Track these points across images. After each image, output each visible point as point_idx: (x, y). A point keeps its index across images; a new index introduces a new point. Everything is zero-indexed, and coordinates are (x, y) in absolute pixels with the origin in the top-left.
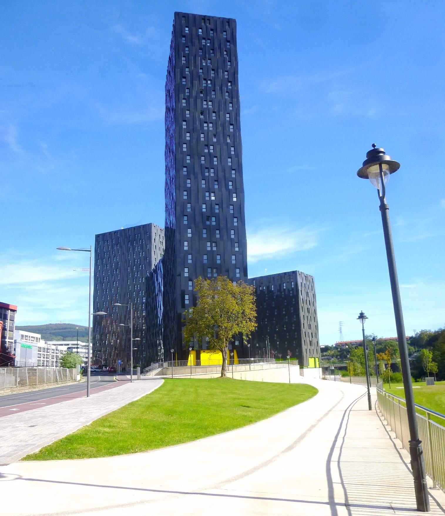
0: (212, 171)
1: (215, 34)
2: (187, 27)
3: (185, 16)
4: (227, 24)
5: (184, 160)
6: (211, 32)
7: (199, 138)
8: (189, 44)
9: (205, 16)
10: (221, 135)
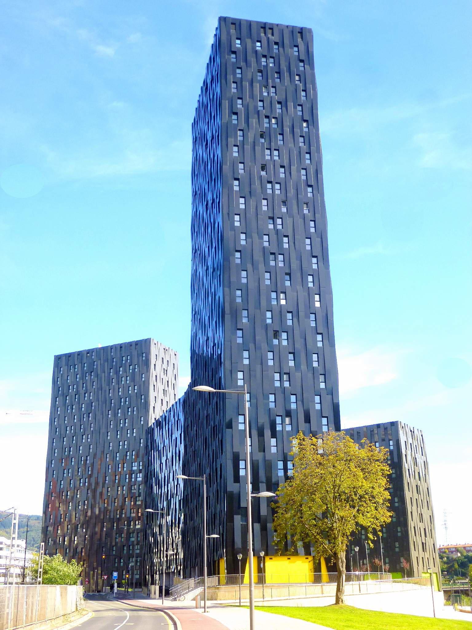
0: (281, 257)
1: (281, 49)
2: (238, 39)
3: (236, 23)
4: (299, 35)
5: (236, 239)
6: (276, 47)
7: (257, 208)
8: (242, 64)
9: (265, 24)
10: (294, 202)
